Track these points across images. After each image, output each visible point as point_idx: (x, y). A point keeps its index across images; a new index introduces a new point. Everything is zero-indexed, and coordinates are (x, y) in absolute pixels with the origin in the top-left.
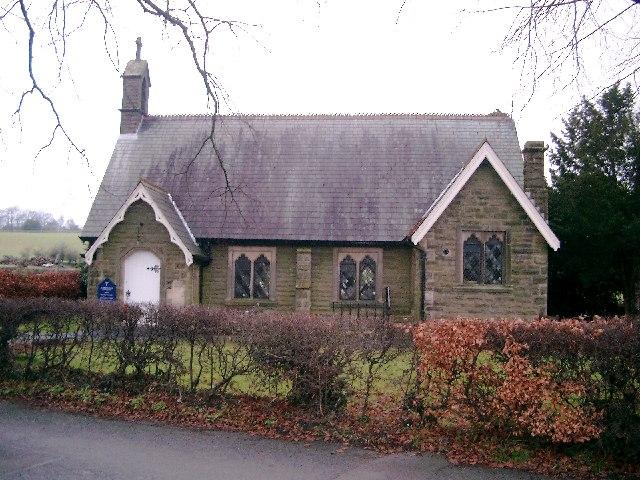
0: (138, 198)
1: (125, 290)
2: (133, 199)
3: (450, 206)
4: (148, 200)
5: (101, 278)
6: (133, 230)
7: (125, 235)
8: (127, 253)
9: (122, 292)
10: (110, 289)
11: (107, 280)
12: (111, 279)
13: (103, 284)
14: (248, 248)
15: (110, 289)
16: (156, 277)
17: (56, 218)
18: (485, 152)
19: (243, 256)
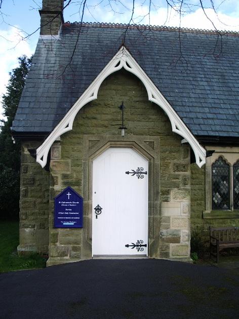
0: (119, 68)
1: (94, 206)
2: (110, 69)
3: (77, 100)
4: (136, 70)
5: (59, 187)
6: (106, 115)
7: (94, 121)
8: (96, 148)
9: (89, 206)
10: (73, 204)
11: (69, 189)
12: (75, 188)
13: (63, 196)
14: (228, 149)
15: (73, 204)
16: (142, 185)
17: (9, 77)
18: (123, 60)
19: (221, 158)
